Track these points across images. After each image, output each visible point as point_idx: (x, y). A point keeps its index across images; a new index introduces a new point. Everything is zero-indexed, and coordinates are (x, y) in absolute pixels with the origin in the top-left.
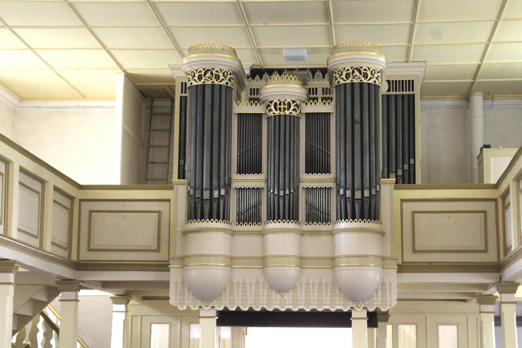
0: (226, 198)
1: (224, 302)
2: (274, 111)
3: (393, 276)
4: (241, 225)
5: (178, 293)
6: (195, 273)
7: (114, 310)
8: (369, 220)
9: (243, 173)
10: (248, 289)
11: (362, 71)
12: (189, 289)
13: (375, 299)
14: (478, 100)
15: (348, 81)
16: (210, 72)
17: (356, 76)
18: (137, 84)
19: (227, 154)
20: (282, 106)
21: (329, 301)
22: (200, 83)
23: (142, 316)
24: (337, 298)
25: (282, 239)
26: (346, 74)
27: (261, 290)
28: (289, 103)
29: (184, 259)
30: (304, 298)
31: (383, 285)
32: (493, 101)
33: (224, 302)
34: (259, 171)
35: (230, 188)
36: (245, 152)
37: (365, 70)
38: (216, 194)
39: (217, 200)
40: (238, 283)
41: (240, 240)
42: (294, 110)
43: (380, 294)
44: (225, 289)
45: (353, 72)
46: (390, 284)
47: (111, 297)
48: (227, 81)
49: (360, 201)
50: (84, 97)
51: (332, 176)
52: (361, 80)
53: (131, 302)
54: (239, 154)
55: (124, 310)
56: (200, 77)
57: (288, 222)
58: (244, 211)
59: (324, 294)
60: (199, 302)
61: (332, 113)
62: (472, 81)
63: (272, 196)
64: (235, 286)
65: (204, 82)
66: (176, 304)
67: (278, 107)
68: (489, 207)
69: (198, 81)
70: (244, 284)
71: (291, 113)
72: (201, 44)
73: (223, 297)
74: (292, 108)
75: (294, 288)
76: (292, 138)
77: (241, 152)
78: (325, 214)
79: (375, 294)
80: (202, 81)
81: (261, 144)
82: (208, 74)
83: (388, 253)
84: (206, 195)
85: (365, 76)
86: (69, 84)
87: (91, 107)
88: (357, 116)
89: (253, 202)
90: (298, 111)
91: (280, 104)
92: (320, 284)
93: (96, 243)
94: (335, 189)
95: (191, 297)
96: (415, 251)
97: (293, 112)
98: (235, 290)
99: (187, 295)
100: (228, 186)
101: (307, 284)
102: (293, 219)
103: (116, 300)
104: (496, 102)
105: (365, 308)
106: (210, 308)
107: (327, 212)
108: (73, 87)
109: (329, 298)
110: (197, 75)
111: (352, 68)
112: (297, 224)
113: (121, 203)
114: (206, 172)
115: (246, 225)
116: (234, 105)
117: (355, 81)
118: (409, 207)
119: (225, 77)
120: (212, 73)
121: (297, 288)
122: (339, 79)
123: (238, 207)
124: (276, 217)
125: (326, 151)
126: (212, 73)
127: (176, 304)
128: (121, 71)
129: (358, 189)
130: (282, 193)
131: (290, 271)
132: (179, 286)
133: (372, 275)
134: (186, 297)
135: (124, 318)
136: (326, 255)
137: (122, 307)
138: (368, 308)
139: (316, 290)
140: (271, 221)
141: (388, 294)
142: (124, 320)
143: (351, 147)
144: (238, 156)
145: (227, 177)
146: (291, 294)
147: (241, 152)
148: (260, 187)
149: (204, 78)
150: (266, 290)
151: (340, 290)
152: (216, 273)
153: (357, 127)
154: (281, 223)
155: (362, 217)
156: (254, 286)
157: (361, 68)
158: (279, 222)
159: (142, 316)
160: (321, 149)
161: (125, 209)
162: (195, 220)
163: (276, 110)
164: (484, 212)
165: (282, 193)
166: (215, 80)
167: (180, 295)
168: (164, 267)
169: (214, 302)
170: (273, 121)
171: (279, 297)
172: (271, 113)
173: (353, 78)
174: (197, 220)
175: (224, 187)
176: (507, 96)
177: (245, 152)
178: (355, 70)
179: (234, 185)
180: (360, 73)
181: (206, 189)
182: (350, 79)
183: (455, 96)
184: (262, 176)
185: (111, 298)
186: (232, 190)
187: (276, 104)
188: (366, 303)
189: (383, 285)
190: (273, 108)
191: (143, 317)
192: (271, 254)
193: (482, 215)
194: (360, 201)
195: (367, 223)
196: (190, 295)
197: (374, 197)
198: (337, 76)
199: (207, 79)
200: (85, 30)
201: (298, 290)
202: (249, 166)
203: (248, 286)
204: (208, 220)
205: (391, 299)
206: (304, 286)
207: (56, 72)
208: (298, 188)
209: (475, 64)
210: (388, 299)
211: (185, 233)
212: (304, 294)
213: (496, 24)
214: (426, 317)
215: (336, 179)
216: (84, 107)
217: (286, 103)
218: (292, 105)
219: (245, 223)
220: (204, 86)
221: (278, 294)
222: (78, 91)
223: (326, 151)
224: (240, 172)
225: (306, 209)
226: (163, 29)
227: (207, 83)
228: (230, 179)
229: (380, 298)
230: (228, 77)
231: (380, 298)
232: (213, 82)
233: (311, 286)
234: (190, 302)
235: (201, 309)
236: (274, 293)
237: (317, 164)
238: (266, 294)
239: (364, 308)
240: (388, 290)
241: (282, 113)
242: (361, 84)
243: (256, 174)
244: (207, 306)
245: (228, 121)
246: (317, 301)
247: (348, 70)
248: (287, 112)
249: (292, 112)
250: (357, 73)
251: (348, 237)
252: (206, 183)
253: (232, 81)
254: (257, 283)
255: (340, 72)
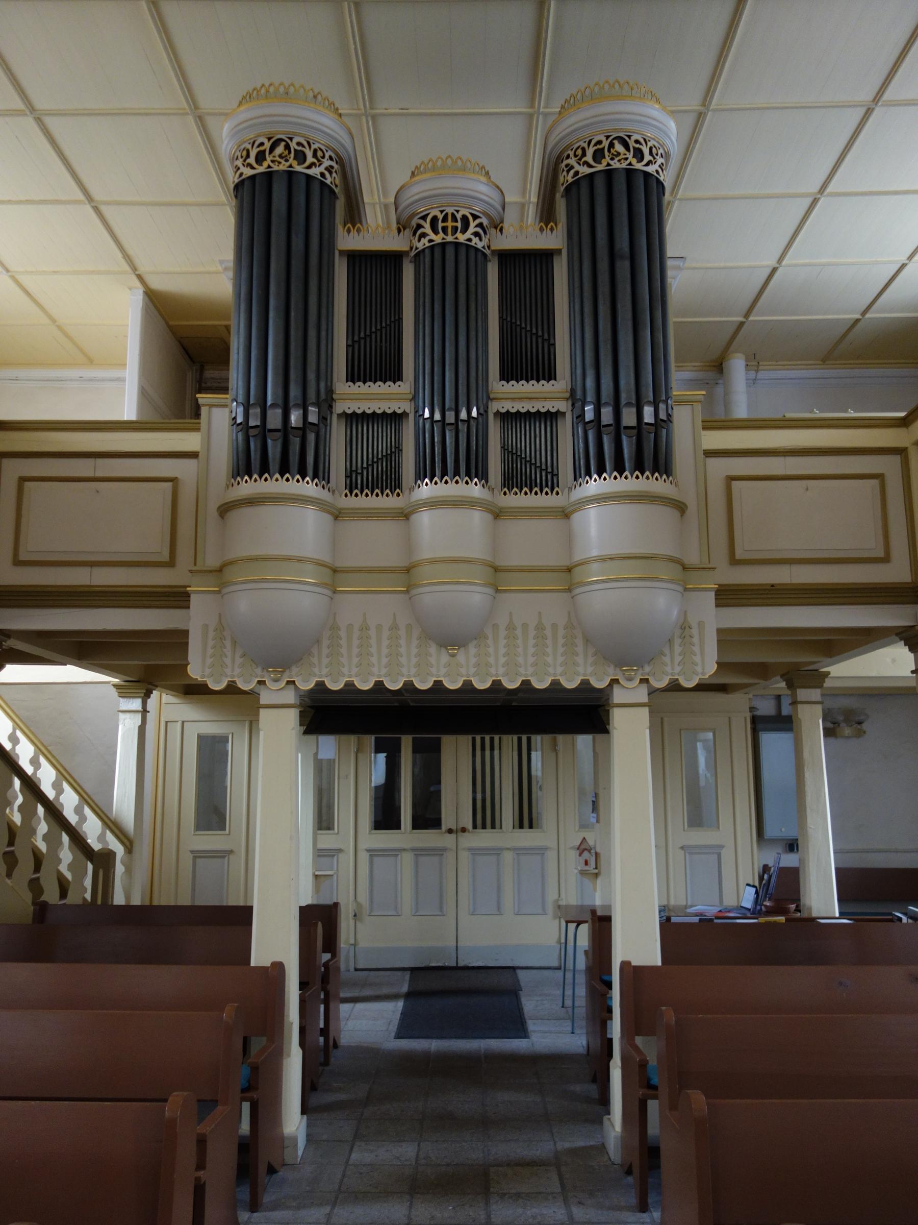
0: (321, 429)
1: (316, 670)
2: (432, 236)
3: (710, 618)
4: (356, 495)
5: (210, 651)
6: (246, 603)
7: (121, 709)
8: (657, 474)
9: (359, 380)
10: (373, 641)
11: (632, 144)
12: (234, 643)
13: (667, 659)
14: (737, 366)
15: (600, 167)
16: (283, 144)
17: (619, 154)
18: (171, 323)
19: (323, 334)
20: (450, 224)
21: (561, 665)
22: (261, 169)
23: (183, 722)
24: (580, 659)
25: (446, 519)
26: (595, 152)
27: (402, 642)
28: (465, 218)
29: (220, 573)
30: (503, 660)
31: (684, 627)
32: (757, 371)
33: (316, 670)
34: (396, 376)
35: (331, 413)
36: (365, 338)
37: (637, 142)
38: (295, 418)
39: (301, 432)
40: (350, 627)
41: (356, 529)
42: (476, 234)
43: (677, 649)
44: (318, 641)
45: (611, 145)
46: (701, 625)
47: (114, 686)
48: (322, 169)
49: (635, 431)
50: (90, 361)
51: (561, 385)
52: (630, 164)
53: (155, 694)
54: (350, 343)
55: (140, 709)
56: (260, 158)
57: (467, 483)
58: (362, 468)
59: (549, 650)
60: (259, 671)
61: (559, 252)
62: (741, 319)
63: (427, 426)
64: (343, 633)
65: (269, 167)
66: (203, 676)
67: (440, 225)
68: (889, 466)
69: (255, 165)
70: (364, 628)
71: (470, 240)
72: (263, 85)
73: (315, 660)
74: (472, 229)
75: (478, 636)
76: (472, 296)
77: (356, 338)
78: (547, 473)
79: (667, 651)
80: (265, 164)
81: (400, 320)
82: (280, 149)
83: (693, 558)
84: (274, 419)
85: (639, 155)
86: (54, 321)
87: (103, 380)
88: (623, 243)
89: (382, 447)
90: (485, 242)
91: (445, 219)
92: (540, 627)
93: (31, 548)
94: (569, 416)
95: (239, 661)
96: (734, 561)
97: (475, 240)
98: (343, 642)
99: (229, 654)
100: (327, 402)
101: (511, 627)
102: (476, 476)
103: (123, 691)
104: (761, 375)
105: (644, 681)
106: (283, 684)
107: (549, 470)
108: (59, 328)
109: (560, 659)
110: (253, 154)
111: (608, 137)
112: (486, 489)
113: (90, 462)
114: (275, 368)
115: (367, 495)
116: (340, 231)
117: (615, 164)
118: (720, 468)
119: (319, 161)
120: (287, 147)
121: (486, 638)
122: (577, 167)
123: (350, 457)
124: (438, 472)
125: (546, 336)
126: (287, 147)
127: (203, 676)
128: (138, 284)
129: (629, 404)
130: (450, 417)
131: (474, 597)
132: (211, 634)
133: (662, 603)
134: (228, 661)
135: (140, 723)
136: (553, 562)
137: (136, 704)
138: (652, 681)
139: (531, 642)
140: (427, 480)
141: (696, 649)
142: (139, 727)
143: (609, 311)
144: (348, 346)
145: (322, 385)
146: (472, 650)
147: (356, 338)
148: (399, 411)
149: (269, 158)
150: (415, 642)
151: (587, 641)
152: (299, 601)
153: (623, 267)
154: (452, 485)
155: (639, 467)
156: (386, 633)
157: (629, 137)
158: (446, 482)
159: (183, 722)
160: (534, 331)
161: (99, 474)
162: (246, 477)
163: (436, 232)
164: (880, 477)
165: (450, 417)
166: (295, 163)
167: (212, 656)
168: (178, 598)
169: (295, 670)
170: (428, 260)
171: (445, 658)
172: (425, 241)
173: (612, 159)
174: (251, 478)
175: (317, 404)
176: (781, 363)
177: (365, 338)
178: (616, 142)
179: (341, 407)
180: (627, 148)
181: (274, 405)
182: (604, 162)
183: (696, 364)
184: (404, 387)
185: (116, 686)
186: (335, 417)
187: (434, 220)
188: (647, 669)
189: (684, 627)
190: (427, 229)
191: (185, 724)
192: (426, 554)
193: (875, 482)
194: (635, 431)
195: (652, 480)
196: (238, 655)
197: (663, 424)
198: (572, 161)
199: (277, 159)
200: (29, 122)
201: (490, 642)
202: (376, 361)
203: (373, 633)
204: (277, 476)
205: (703, 660)
206: (503, 633)
207: (13, 278)
208: (486, 412)
209: (767, 266)
210: (697, 659)
211: (225, 510)
212: (502, 651)
213: (869, 112)
214: (662, 719)
215: (573, 391)
216: (91, 380)
217: (459, 216)
218: (472, 224)
219: (366, 491)
220: (269, 175)
221: (443, 650)
222: (81, 350)
223: (546, 336)
224: (352, 377)
225: (503, 461)
226: (190, 119)
227: (275, 168)
228: (330, 391)
229: (678, 659)
230: (327, 163)
231: (678, 659)
232: (291, 166)
233: (519, 632)
234: (237, 671)
235: (262, 686)
236: (433, 649)
237: (527, 359)
238: (414, 651)
239: (642, 681)
240: (696, 640)
241: (450, 238)
242: (630, 172)
243: (389, 383)
244: (276, 680)
245: (324, 288)
246: (532, 666)
247: (600, 142)
248: (462, 238)
249: (472, 237)
250: (619, 147)
251: (603, 516)
252: (274, 393)
253: (334, 175)
254: (394, 627)
255: (579, 152)
